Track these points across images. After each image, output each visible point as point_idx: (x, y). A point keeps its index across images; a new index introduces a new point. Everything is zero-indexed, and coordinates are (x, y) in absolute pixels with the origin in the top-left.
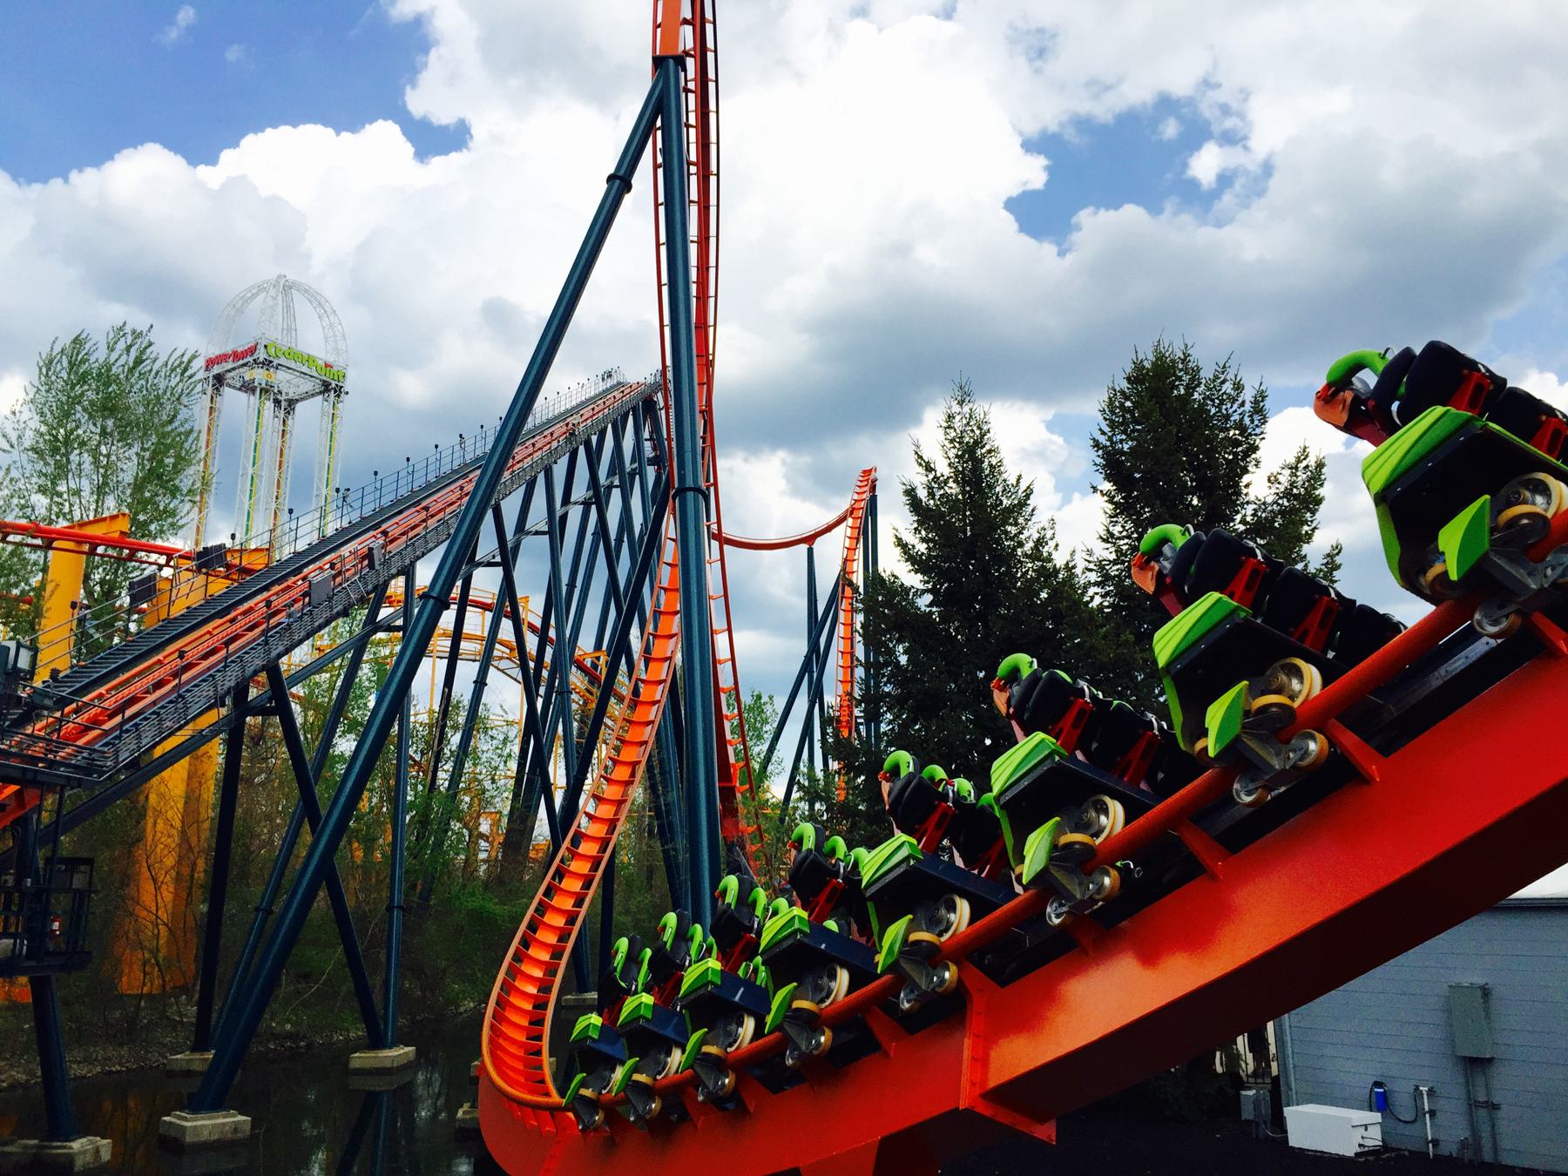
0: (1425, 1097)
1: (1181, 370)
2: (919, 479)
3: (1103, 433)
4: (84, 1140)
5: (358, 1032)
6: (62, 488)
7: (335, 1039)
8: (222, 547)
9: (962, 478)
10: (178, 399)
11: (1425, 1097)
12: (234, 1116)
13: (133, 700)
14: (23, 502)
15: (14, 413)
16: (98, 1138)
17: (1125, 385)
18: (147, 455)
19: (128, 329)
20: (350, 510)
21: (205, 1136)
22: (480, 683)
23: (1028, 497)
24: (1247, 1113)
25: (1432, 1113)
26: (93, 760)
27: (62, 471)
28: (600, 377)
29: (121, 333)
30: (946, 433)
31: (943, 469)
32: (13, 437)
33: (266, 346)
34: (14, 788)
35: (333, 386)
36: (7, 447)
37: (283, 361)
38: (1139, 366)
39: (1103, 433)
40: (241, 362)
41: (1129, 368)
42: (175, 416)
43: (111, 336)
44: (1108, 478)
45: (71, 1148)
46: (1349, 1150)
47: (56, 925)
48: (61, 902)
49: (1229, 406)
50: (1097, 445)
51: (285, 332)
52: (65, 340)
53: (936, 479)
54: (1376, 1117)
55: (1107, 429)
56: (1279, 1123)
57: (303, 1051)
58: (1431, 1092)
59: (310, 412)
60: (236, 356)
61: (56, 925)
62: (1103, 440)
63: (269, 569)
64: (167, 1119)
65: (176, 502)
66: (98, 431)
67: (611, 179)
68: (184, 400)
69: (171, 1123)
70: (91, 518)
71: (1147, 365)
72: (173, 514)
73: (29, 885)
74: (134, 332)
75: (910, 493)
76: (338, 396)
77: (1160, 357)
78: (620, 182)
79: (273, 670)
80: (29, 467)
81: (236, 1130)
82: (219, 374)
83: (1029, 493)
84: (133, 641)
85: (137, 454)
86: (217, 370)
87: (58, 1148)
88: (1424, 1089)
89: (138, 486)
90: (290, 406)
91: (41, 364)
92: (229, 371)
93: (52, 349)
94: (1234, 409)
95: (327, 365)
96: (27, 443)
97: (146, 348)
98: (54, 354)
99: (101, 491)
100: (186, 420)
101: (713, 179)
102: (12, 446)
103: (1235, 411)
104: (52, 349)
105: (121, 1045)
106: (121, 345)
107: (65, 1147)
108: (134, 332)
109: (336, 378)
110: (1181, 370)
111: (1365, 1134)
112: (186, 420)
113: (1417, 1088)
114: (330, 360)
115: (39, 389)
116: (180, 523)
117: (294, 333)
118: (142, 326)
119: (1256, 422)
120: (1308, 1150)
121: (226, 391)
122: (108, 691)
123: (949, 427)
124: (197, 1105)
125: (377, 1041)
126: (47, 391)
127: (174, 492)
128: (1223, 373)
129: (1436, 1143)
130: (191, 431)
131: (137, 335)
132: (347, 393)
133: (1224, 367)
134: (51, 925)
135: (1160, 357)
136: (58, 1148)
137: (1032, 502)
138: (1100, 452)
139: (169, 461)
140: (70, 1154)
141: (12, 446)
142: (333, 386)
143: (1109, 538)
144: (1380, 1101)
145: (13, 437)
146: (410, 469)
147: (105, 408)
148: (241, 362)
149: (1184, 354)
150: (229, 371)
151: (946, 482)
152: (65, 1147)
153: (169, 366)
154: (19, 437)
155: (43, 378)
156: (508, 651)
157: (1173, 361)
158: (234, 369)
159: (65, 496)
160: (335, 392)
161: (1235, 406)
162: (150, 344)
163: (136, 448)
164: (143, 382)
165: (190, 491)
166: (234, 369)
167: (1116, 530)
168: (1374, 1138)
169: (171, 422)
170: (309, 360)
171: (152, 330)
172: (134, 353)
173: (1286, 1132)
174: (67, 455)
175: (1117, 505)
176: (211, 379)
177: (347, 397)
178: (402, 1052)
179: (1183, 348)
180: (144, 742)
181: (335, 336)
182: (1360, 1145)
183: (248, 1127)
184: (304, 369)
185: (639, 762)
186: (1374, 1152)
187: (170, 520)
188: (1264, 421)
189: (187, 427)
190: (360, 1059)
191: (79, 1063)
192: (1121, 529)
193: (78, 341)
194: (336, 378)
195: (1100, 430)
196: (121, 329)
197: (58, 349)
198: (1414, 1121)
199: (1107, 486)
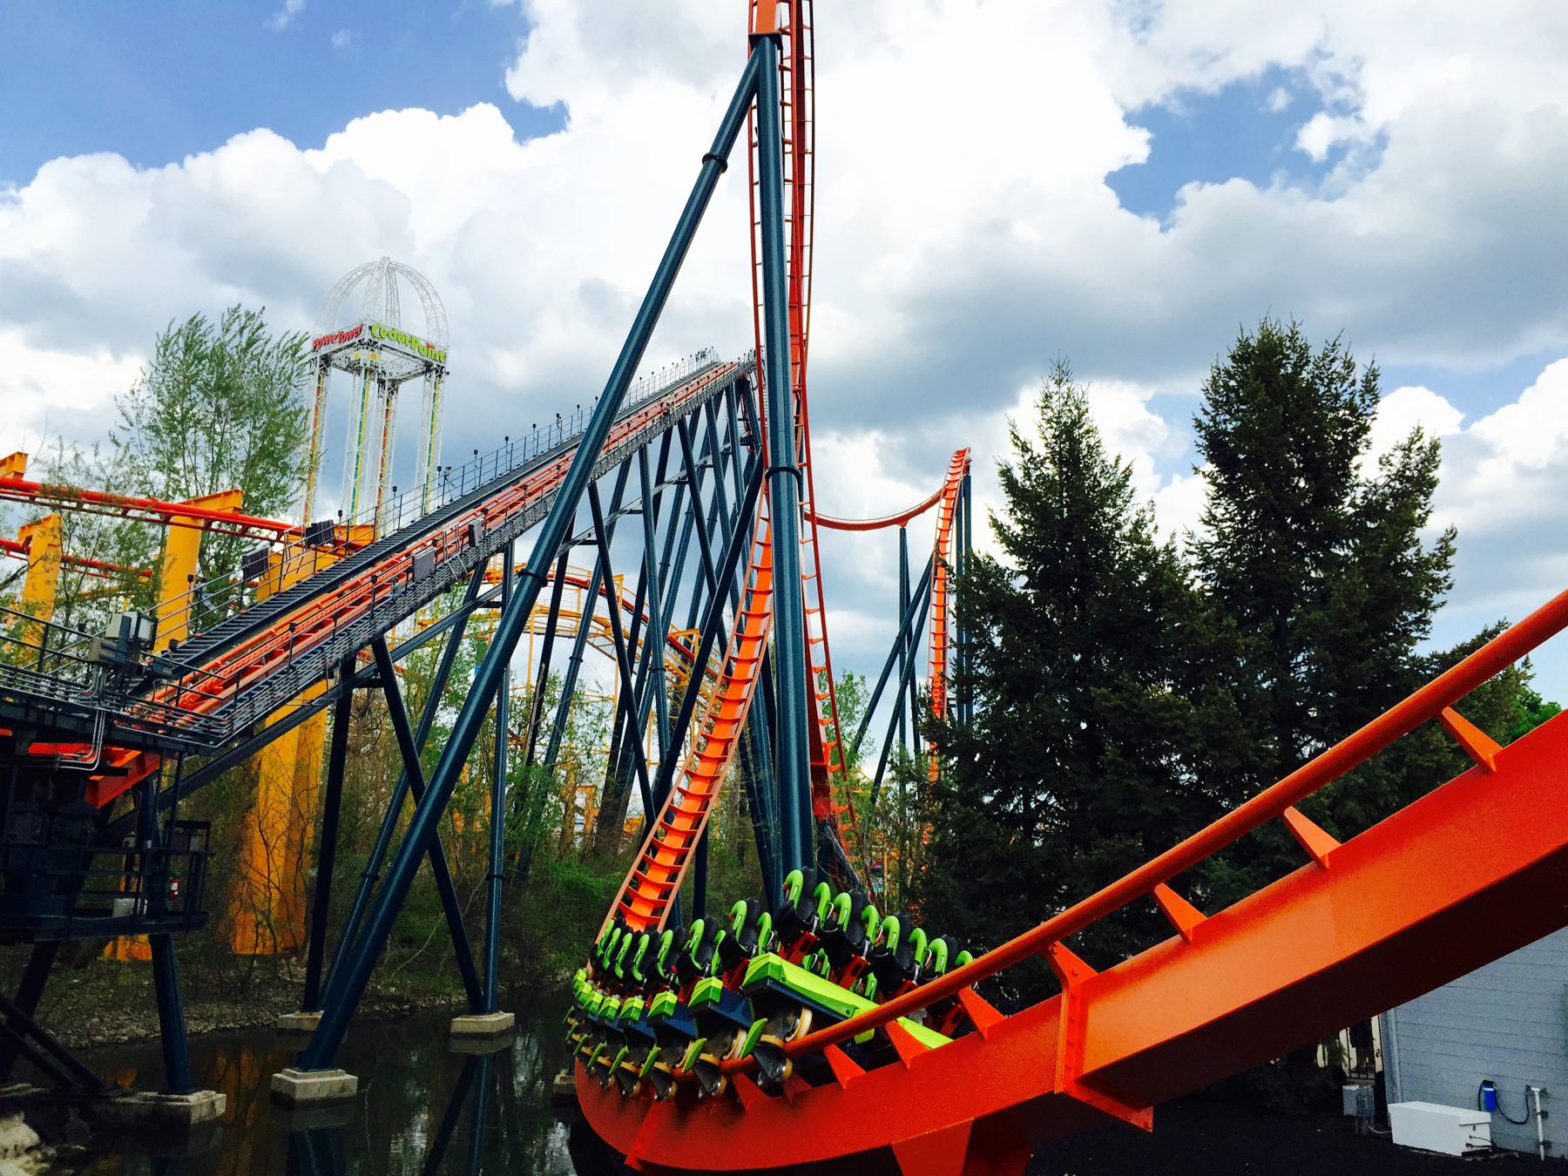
0: (1537, 1098)
1: (1289, 348)
2: (1015, 461)
3: (1206, 413)
4: (199, 1094)
5: (459, 997)
6: (179, 465)
7: (438, 1002)
8: (329, 523)
9: (1059, 459)
10: (289, 378)
11: (1537, 1098)
12: (341, 1074)
13: (246, 671)
14: (141, 478)
15: (133, 392)
16: (213, 1092)
17: (1229, 364)
18: (259, 433)
19: (242, 312)
20: (451, 488)
21: (312, 1094)
22: (576, 659)
23: (1127, 478)
24: (1350, 1108)
25: (1544, 1115)
26: (210, 727)
27: (179, 449)
28: (694, 357)
29: (236, 315)
30: (1043, 413)
31: (1039, 449)
32: (132, 415)
33: (370, 328)
34: (134, 753)
35: (435, 366)
36: (127, 425)
37: (386, 342)
38: (1244, 345)
39: (1206, 413)
40: (347, 343)
41: (1234, 347)
42: (285, 396)
43: (226, 317)
44: (1211, 459)
45: (188, 1101)
46: (1456, 1150)
47: (175, 886)
48: (178, 865)
49: (1339, 385)
50: (1199, 425)
51: (389, 313)
52: (182, 322)
53: (1032, 459)
54: (1486, 1116)
55: (1210, 409)
56: (1383, 1119)
57: (407, 1013)
58: (1543, 1093)
59: (413, 391)
60: (342, 337)
61: (175, 886)
62: (1206, 420)
63: (375, 545)
64: (278, 1075)
65: (285, 479)
66: (213, 410)
67: (707, 158)
68: (295, 380)
69: (281, 1080)
70: (206, 494)
71: (1253, 343)
72: (283, 490)
73: (149, 847)
74: (247, 314)
75: (1006, 473)
76: (440, 376)
77: (1267, 335)
78: (716, 162)
79: (378, 643)
80: (147, 444)
81: (343, 1089)
82: (326, 355)
83: (1127, 475)
84: (247, 614)
85: (249, 432)
86: (324, 350)
87: (177, 1101)
88: (1536, 1090)
89: (251, 463)
90: (393, 386)
91: (159, 344)
92: (335, 352)
93: (169, 331)
94: (1344, 388)
95: (428, 346)
96: (145, 422)
97: (258, 329)
98: (171, 335)
99: (216, 467)
100: (296, 401)
101: (808, 158)
102: (132, 425)
103: (1346, 390)
104: (169, 331)
105: (236, 1002)
106: (236, 327)
107: (182, 1100)
108: (247, 314)
109: (437, 358)
110: (1289, 348)
111: (1473, 1134)
112: (296, 401)
113: (1528, 1088)
114: (432, 340)
115: (156, 369)
116: (290, 500)
117: (397, 314)
118: (256, 310)
119: (1367, 402)
120: (1413, 1148)
121: (333, 371)
122: (223, 661)
123: (1046, 407)
124: (307, 1063)
125: (477, 1006)
126: (164, 371)
127: (284, 469)
128: (1333, 351)
129: (1547, 1145)
130: (301, 410)
131: (250, 317)
132: (448, 373)
133: (1334, 345)
134: (170, 887)
135: (1267, 335)
136: (177, 1101)
137: (1131, 483)
138: (1203, 433)
139: (280, 439)
140: (186, 1106)
141: (132, 425)
142: (435, 366)
143: (1211, 520)
144: (1490, 1100)
145: (132, 415)
146: (509, 449)
147: (218, 387)
148: (347, 343)
149: (1292, 332)
150: (335, 352)
151: (1042, 463)
152: (182, 1100)
153: (281, 347)
154: (138, 415)
155: (161, 359)
156: (603, 628)
157: (1280, 339)
158: (340, 350)
159: (182, 473)
160: (437, 372)
161: (1345, 385)
162: (262, 325)
163: (248, 428)
164: (255, 363)
165: (299, 469)
166: (340, 350)
167: (1219, 512)
168: (1483, 1138)
169: (282, 401)
170: (411, 341)
171: (265, 312)
172: (246, 333)
173: (1390, 1129)
174: (183, 433)
175: (1220, 486)
176: (318, 359)
177: (448, 377)
178: (501, 1017)
179: (1291, 325)
180: (257, 711)
181: (436, 317)
182: (1468, 1145)
183: (354, 1088)
184: (407, 350)
185: (732, 740)
186: (1483, 1152)
187: (280, 497)
188: (1376, 400)
189: (297, 406)
190: (462, 1024)
191: (196, 1019)
192: (1224, 512)
193: (195, 324)
194: (437, 358)
195: (1203, 410)
196: (235, 310)
197: (174, 330)
198: (1522, 1123)
199: (1210, 467)
